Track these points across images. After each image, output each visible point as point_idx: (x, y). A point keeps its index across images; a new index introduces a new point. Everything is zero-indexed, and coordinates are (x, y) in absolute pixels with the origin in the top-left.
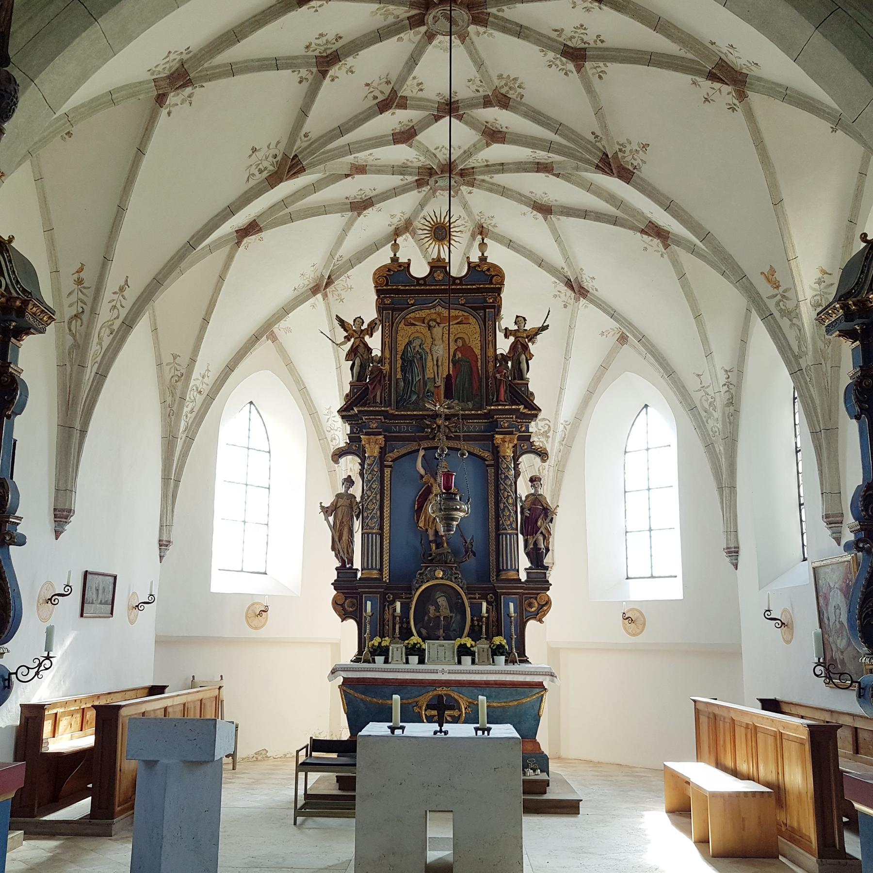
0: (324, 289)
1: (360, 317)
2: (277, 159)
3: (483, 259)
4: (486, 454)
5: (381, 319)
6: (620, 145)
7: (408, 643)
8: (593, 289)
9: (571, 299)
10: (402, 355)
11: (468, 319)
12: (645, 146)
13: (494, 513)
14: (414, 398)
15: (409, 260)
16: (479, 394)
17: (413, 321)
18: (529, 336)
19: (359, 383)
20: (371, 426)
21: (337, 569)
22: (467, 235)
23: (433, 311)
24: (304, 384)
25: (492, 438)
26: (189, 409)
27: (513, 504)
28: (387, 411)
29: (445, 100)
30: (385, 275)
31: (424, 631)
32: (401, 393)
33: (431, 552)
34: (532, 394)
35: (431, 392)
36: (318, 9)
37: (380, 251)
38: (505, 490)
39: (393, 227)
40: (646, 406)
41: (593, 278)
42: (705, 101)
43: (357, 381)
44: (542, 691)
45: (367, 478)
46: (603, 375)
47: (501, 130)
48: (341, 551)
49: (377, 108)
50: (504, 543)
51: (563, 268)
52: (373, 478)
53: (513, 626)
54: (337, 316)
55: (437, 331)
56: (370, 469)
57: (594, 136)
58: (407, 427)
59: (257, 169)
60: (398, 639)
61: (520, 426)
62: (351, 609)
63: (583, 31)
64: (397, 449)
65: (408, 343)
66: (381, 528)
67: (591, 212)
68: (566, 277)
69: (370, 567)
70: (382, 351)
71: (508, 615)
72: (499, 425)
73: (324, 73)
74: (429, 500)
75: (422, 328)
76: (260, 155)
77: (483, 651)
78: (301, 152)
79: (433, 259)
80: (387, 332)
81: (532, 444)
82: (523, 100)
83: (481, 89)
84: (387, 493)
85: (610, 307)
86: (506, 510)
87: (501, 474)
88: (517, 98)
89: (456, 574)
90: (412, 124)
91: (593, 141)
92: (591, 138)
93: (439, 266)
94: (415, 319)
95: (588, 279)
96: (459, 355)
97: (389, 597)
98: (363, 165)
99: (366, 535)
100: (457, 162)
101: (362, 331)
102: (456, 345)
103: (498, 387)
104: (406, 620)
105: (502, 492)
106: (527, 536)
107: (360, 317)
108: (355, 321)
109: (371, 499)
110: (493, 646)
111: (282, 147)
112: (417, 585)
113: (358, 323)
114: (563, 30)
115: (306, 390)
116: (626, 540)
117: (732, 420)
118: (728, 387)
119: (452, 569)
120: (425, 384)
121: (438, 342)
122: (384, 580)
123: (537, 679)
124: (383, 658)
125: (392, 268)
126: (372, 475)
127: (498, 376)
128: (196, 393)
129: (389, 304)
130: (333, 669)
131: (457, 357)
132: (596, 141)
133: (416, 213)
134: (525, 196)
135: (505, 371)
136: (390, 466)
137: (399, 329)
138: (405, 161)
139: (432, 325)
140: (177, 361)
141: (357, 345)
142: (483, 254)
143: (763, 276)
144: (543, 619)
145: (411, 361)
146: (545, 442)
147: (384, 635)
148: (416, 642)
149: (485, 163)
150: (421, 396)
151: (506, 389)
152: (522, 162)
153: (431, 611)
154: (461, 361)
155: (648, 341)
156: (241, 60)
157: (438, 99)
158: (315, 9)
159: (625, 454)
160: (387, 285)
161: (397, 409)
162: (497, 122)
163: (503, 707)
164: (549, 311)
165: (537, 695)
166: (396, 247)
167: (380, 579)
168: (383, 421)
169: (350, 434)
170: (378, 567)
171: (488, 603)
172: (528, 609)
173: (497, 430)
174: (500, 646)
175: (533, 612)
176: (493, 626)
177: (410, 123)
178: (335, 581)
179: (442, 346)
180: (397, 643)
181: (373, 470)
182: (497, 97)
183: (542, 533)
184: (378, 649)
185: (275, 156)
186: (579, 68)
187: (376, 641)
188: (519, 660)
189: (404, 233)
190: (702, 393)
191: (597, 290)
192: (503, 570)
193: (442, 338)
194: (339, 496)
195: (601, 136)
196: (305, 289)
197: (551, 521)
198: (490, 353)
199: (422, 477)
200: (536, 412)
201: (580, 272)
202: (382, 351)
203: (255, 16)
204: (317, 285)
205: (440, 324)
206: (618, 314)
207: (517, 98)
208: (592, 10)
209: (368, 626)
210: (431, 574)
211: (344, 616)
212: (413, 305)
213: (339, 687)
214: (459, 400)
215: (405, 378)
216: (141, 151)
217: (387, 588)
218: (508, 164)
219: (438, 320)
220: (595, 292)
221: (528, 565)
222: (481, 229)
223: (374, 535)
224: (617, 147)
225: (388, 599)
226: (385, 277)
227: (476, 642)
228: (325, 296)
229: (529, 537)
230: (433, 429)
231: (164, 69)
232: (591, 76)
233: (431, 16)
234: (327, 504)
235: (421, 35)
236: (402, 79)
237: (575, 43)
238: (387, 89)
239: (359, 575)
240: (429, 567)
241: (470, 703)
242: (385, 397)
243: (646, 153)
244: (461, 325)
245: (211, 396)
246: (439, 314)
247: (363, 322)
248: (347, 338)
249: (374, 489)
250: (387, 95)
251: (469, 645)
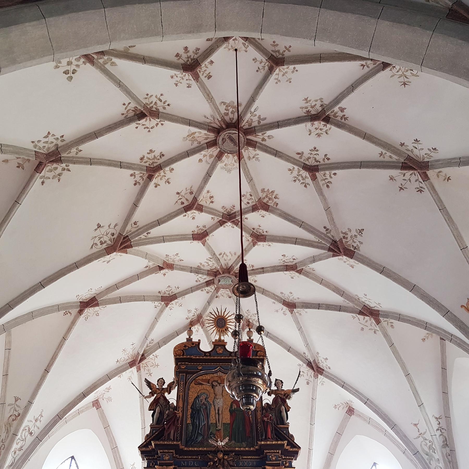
2: (114, 237)
5: (177, 380)
6: (344, 233)
8: (327, 368)
12: (361, 231)
14: (200, 438)
15: (199, 340)
18: (286, 394)
23: (215, 375)
24: (116, 444)
26: (19, 446)
29: (227, 212)
34: (292, 436)
36: (151, 130)
37: (180, 336)
39: (189, 320)
40: (375, 464)
41: (327, 359)
42: (400, 190)
43: (156, 424)
47: (263, 234)
49: (183, 209)
51: (304, 353)
57: (325, 229)
58: (194, 462)
59: (99, 241)
63: (316, 152)
65: (196, 397)
68: (307, 360)
70: (177, 401)
72: (268, 458)
73: (150, 178)
75: (207, 387)
76: (103, 230)
78: (130, 234)
79: (216, 340)
80: (182, 386)
82: (277, 207)
83: (250, 202)
85: (340, 380)
88: (274, 205)
90: (205, 229)
91: (325, 233)
92: (324, 231)
93: (219, 344)
94: (203, 380)
95: (323, 360)
98: (172, 264)
100: (233, 265)
101: (163, 389)
108: (158, 381)
111: (118, 228)
113: (160, 382)
114: (303, 153)
115: (118, 449)
117: (450, 459)
118: (441, 431)
120: (209, 428)
125: (187, 345)
127: (265, 419)
128: (27, 433)
129: (184, 369)
131: (233, 408)
132: (327, 233)
133: (205, 309)
134: (277, 296)
135: (270, 415)
137: (190, 387)
138: (200, 265)
139: (214, 384)
140: (18, 403)
141: (158, 397)
143: (463, 308)
145: (198, 410)
149: (252, 268)
150: (206, 437)
151: (272, 430)
152: (276, 266)
155: (372, 402)
156: (97, 158)
157: (222, 210)
158: (148, 129)
160: (183, 355)
161: (186, 446)
162: (260, 228)
166: (190, 333)
173: (267, 462)
177: (204, 228)
182: (261, 203)
185: (113, 234)
186: (314, 178)
189: (196, 324)
190: (421, 439)
191: (329, 368)
193: (222, 394)
195: (330, 229)
196: (125, 362)
200: (296, 449)
202: (177, 401)
203: (109, 126)
204: (134, 360)
206: (347, 384)
207: (274, 205)
208: (321, 135)
212: (201, 370)
214: (235, 441)
215: (193, 423)
216: (17, 202)
218: (266, 268)
219: (219, 381)
220: (328, 370)
222: (248, 323)
224: (342, 235)
226: (182, 350)
228: (139, 369)
230: (215, 462)
231: (44, 147)
232: (321, 185)
233: (221, 138)
235: (213, 158)
236: (201, 189)
237: (311, 162)
238: (190, 198)
242: (177, 437)
243: (362, 236)
245: (39, 439)
246: (220, 377)
247: (164, 383)
248: (152, 394)
250: (190, 202)
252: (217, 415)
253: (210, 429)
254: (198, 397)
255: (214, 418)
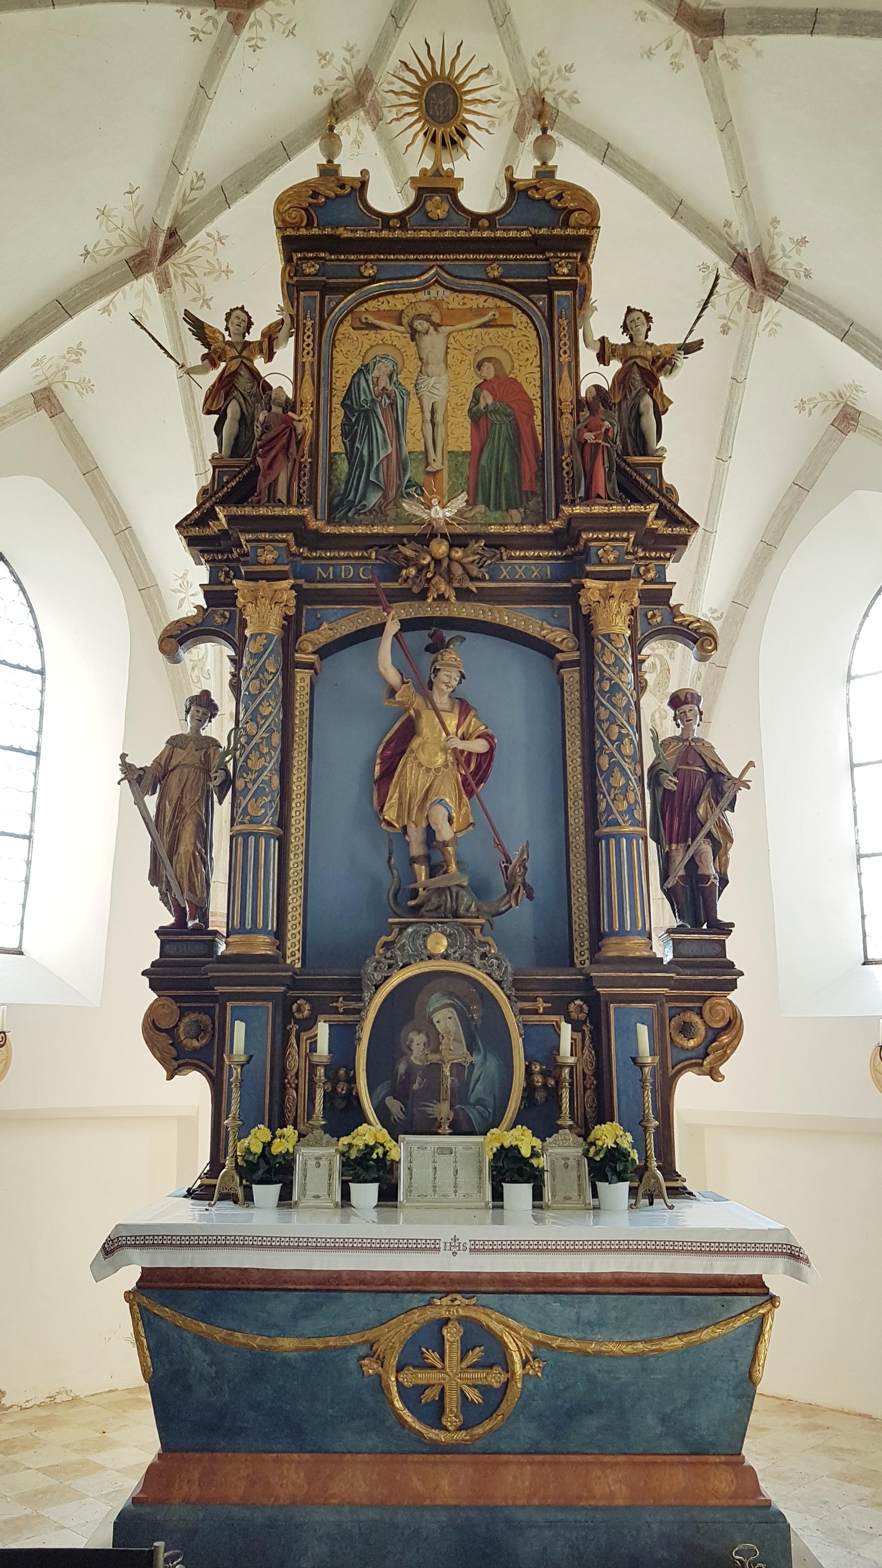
0: (161, 262)
1: (242, 308)
3: (546, 173)
4: (558, 636)
5: (294, 312)
7: (350, 1146)
9: (740, 309)
10: (344, 399)
11: (508, 315)
13: (580, 785)
14: (374, 498)
15: (364, 172)
16: (538, 490)
17: (371, 319)
18: (659, 357)
19: (235, 461)
20: (262, 559)
21: (161, 932)
22: (505, 130)
23: (422, 296)
25: (573, 596)
27: (632, 757)
28: (302, 518)
30: (306, 205)
31: (394, 1106)
32: (343, 487)
33: (413, 886)
34: (671, 490)
35: (416, 485)
38: (612, 719)
43: (231, 456)
44: (760, 1305)
45: (247, 689)
46: (800, 503)
48: (174, 884)
50: (613, 860)
51: (728, 224)
52: (261, 690)
53: (648, 1093)
54: (186, 312)
55: (433, 342)
56: (254, 666)
60: (319, 1132)
61: (643, 568)
62: (196, 1044)
64: (330, 623)
65: (360, 371)
66: (283, 821)
67: (829, 11)
69: (248, 926)
71: (634, 1060)
74: (412, 751)
77: (566, 1166)
80: (310, 341)
81: (674, 611)
84: (300, 732)
85: (840, 314)
86: (617, 772)
87: (600, 681)
89: (483, 944)
94: (379, 314)
95: (789, 246)
96: (487, 399)
97: (299, 1010)
99: (240, 840)
102: (480, 376)
103: (588, 467)
104: (347, 1073)
105: (605, 726)
106: (670, 843)
107: (242, 308)
108: (228, 316)
109: (257, 745)
110: (597, 1153)
112: (378, 976)
113: (236, 321)
116: (860, 875)
119: (472, 930)
120: (403, 467)
121: (435, 367)
122: (289, 961)
123: (745, 1267)
124: (275, 1189)
126: (261, 681)
127: (589, 436)
130: (110, 1240)
131: (482, 405)
136: (310, 666)
137: (339, 336)
139: (419, 328)
142: (544, 164)
144: (722, 1069)
145: (366, 412)
146: (667, 658)
147: (282, 1115)
148: (371, 1143)
150: (392, 494)
153: (414, 1047)
154: (496, 412)
159: (848, 681)
160: (310, 224)
161: (330, 521)
163: (641, 1355)
164: (717, 278)
165: (746, 1318)
167: (276, 959)
168: (294, 549)
169: (210, 584)
170: (272, 925)
171: (576, 1027)
172: (681, 1040)
174: (616, 1154)
175: (693, 1048)
176: (585, 1089)
178: (154, 964)
179: (444, 377)
180: (317, 1143)
181: (263, 670)
183: (709, 835)
184: (262, 1164)
187: (261, 1134)
188: (667, 1188)
192: (612, 933)
194: (175, 742)
196: (112, 259)
197: (731, 807)
198: (565, 393)
199: (392, 692)
200: (683, 530)
201: (768, 231)
204: (143, 252)
205: (440, 325)
209: (236, 1095)
210: (415, 945)
211: (175, 1064)
212: (373, 280)
213: (128, 1295)
214: (488, 505)
215: (351, 454)
217: (294, 983)
219: (436, 318)
220: (803, 282)
221: (673, 922)
222: (539, 106)
223: (263, 840)
225: (298, 1016)
226: (305, 209)
227: (543, 1140)
228: (164, 284)
229: (674, 846)
230: (421, 569)
234: (144, 759)
239: (222, 948)
240: (409, 924)
241: (537, 1344)
244: (490, 330)
246: (437, 304)
247: (250, 324)
248: (211, 360)
249: (266, 718)
251: (526, 1152)
252: (429, 427)
253: (405, 470)
254: (365, 370)
255: (419, 436)
